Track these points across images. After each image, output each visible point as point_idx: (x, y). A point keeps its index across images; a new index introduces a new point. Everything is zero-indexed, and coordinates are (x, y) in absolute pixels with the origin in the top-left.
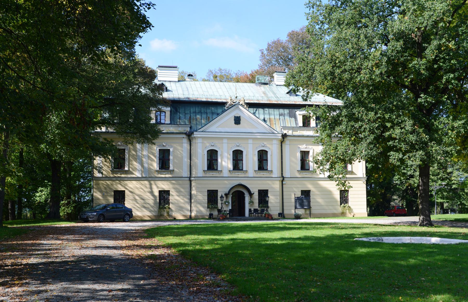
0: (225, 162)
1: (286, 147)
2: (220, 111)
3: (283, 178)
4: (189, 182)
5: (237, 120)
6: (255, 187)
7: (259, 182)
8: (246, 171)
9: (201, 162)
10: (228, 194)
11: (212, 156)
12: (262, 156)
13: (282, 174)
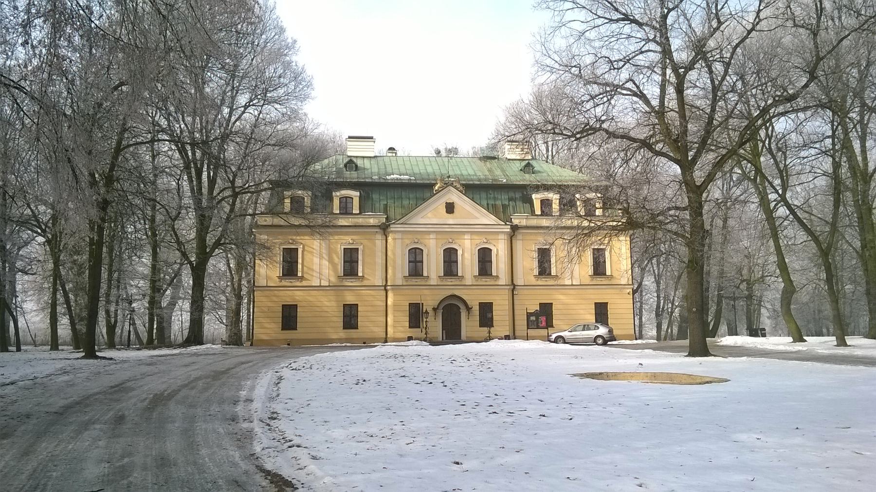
0: (433, 266)
1: (518, 245)
2: (428, 195)
3: (513, 286)
4: (384, 293)
5: (450, 208)
6: (474, 298)
7: (478, 292)
8: (462, 277)
10: (437, 308)
11: (416, 258)
12: (485, 257)
13: (512, 280)
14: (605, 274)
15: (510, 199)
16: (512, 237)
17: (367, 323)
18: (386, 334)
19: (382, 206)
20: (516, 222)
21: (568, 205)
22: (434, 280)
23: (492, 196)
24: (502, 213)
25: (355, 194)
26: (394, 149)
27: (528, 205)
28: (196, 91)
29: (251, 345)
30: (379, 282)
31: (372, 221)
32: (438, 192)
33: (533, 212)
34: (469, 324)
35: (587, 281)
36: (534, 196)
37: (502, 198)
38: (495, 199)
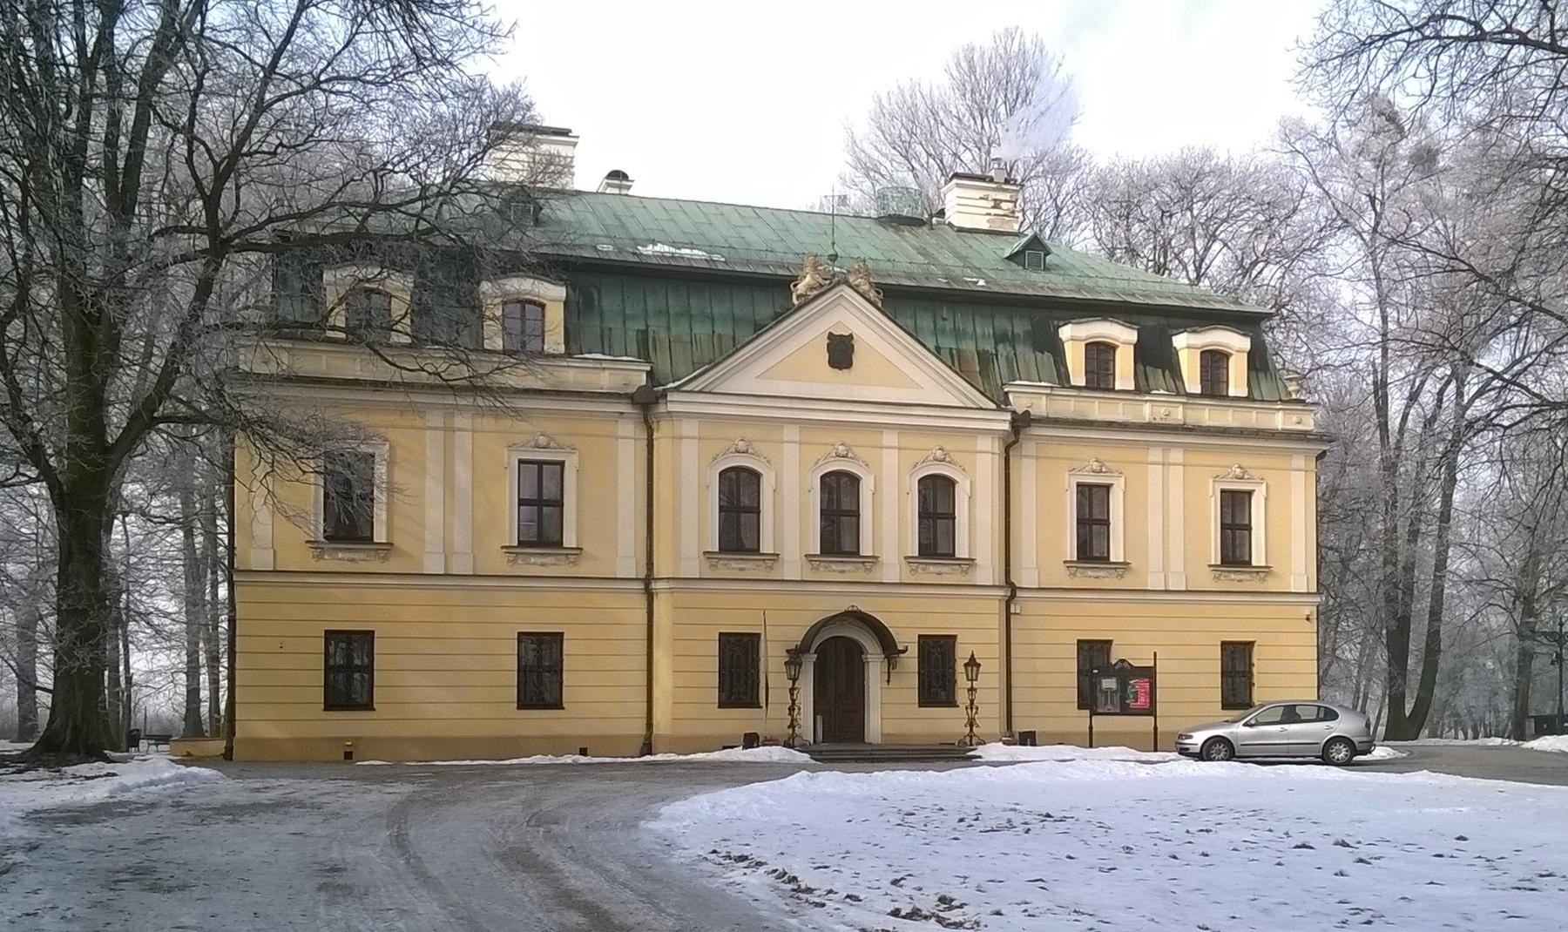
0: (791, 519)
1: (1026, 471)
3: (1012, 590)
5: (841, 352)
9: (694, 518)
11: (739, 497)
12: (936, 498)
14: (370, 540)
15: (1000, 338)
16: (1010, 444)
17: (597, 692)
18: (650, 725)
19: (632, 334)
20: (1019, 403)
21: (1155, 358)
22: (793, 567)
23: (949, 325)
24: (983, 373)
25: (553, 293)
26: (625, 177)
27: (1047, 358)
28: (200, 411)
29: (228, 755)
30: (628, 565)
31: (605, 380)
32: (806, 301)
33: (1063, 379)
34: (889, 704)
35: (1206, 580)
36: (1066, 332)
37: (980, 332)
38: (958, 334)
